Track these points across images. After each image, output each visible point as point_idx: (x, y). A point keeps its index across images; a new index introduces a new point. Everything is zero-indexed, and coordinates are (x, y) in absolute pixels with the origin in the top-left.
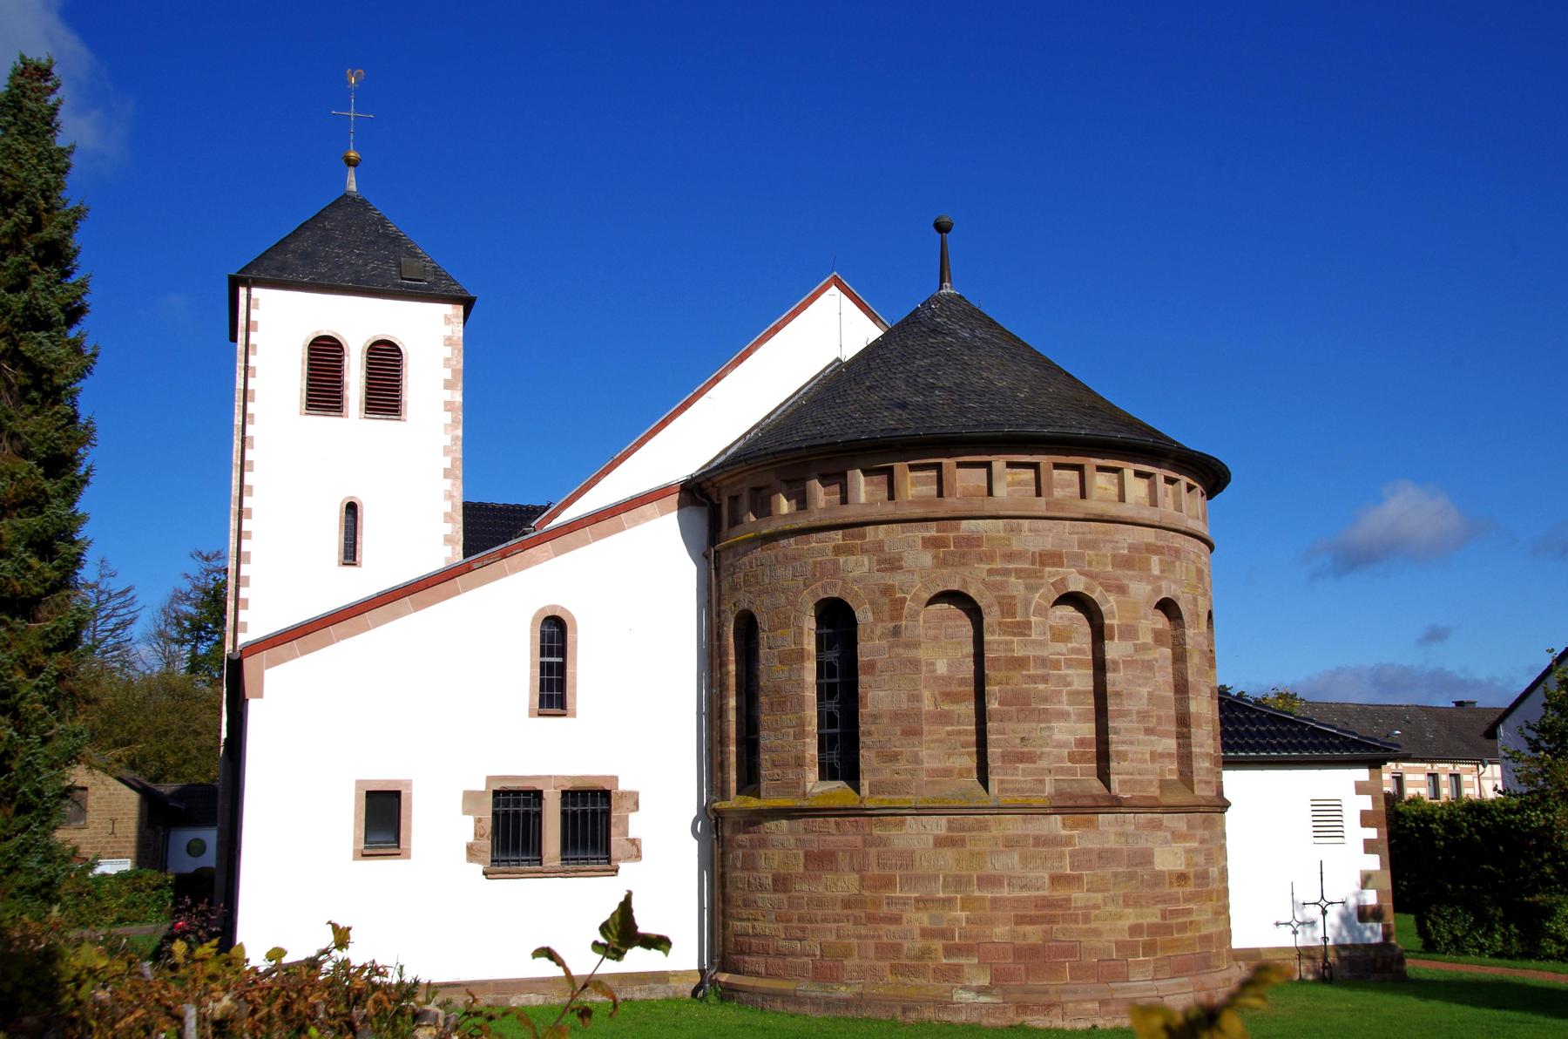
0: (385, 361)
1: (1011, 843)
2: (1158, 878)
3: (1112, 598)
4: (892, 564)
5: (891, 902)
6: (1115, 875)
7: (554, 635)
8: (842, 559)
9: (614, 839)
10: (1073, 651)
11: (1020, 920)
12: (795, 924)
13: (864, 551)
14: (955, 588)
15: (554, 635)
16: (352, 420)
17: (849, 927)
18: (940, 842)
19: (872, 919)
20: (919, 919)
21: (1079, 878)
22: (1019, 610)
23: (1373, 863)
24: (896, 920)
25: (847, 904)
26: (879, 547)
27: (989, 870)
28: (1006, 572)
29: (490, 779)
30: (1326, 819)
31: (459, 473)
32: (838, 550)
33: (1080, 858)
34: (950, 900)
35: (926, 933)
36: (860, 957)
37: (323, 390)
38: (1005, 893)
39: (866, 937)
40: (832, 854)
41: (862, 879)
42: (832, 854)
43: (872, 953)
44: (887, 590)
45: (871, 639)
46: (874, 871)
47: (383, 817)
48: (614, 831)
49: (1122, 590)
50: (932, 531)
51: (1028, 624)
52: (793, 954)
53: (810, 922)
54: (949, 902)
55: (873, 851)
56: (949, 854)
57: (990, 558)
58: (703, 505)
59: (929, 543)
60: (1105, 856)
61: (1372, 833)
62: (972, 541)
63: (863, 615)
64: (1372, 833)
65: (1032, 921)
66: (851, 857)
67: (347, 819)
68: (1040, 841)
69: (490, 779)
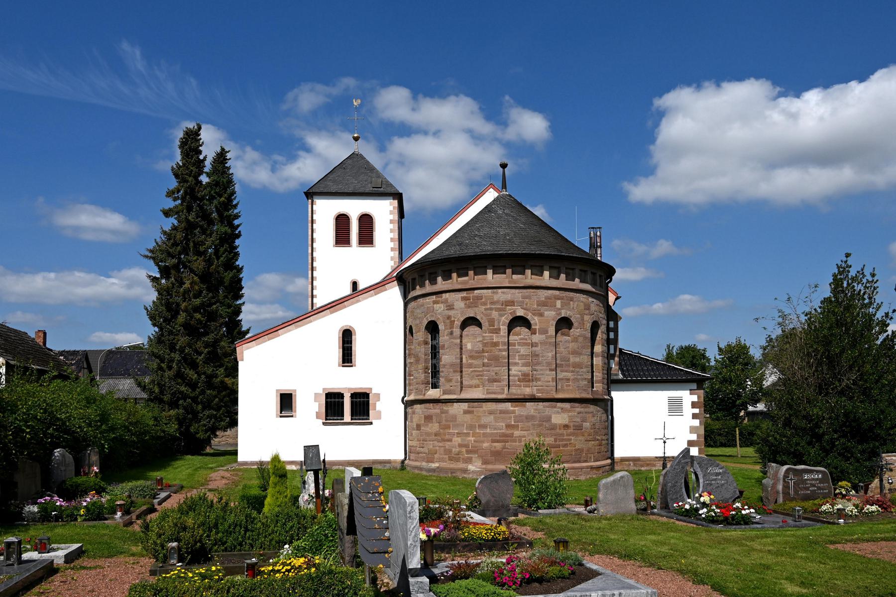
0: (366, 221)
1: (491, 413)
2: (553, 427)
3: (536, 318)
4: (450, 307)
5: (449, 434)
6: (533, 425)
7: (347, 336)
9: (371, 412)
10: (521, 339)
11: (493, 441)
14: (472, 315)
15: (347, 336)
16: (355, 250)
18: (466, 412)
19: (444, 440)
20: (457, 440)
21: (518, 426)
22: (496, 323)
23: (697, 423)
24: (450, 440)
26: (446, 301)
27: (482, 422)
28: (491, 309)
29: (324, 389)
30: (675, 407)
33: (519, 419)
34: (469, 434)
35: (460, 446)
37: (342, 238)
38: (488, 431)
44: (449, 317)
46: (444, 423)
47: (286, 402)
48: (371, 408)
49: (541, 315)
50: (464, 294)
51: (500, 329)
54: (467, 434)
55: (443, 415)
56: (468, 416)
57: (485, 304)
59: (464, 299)
60: (529, 418)
61: (697, 411)
62: (479, 298)
63: (441, 327)
64: (697, 411)
65: (498, 441)
67: (274, 403)
68: (502, 412)
69: (324, 389)
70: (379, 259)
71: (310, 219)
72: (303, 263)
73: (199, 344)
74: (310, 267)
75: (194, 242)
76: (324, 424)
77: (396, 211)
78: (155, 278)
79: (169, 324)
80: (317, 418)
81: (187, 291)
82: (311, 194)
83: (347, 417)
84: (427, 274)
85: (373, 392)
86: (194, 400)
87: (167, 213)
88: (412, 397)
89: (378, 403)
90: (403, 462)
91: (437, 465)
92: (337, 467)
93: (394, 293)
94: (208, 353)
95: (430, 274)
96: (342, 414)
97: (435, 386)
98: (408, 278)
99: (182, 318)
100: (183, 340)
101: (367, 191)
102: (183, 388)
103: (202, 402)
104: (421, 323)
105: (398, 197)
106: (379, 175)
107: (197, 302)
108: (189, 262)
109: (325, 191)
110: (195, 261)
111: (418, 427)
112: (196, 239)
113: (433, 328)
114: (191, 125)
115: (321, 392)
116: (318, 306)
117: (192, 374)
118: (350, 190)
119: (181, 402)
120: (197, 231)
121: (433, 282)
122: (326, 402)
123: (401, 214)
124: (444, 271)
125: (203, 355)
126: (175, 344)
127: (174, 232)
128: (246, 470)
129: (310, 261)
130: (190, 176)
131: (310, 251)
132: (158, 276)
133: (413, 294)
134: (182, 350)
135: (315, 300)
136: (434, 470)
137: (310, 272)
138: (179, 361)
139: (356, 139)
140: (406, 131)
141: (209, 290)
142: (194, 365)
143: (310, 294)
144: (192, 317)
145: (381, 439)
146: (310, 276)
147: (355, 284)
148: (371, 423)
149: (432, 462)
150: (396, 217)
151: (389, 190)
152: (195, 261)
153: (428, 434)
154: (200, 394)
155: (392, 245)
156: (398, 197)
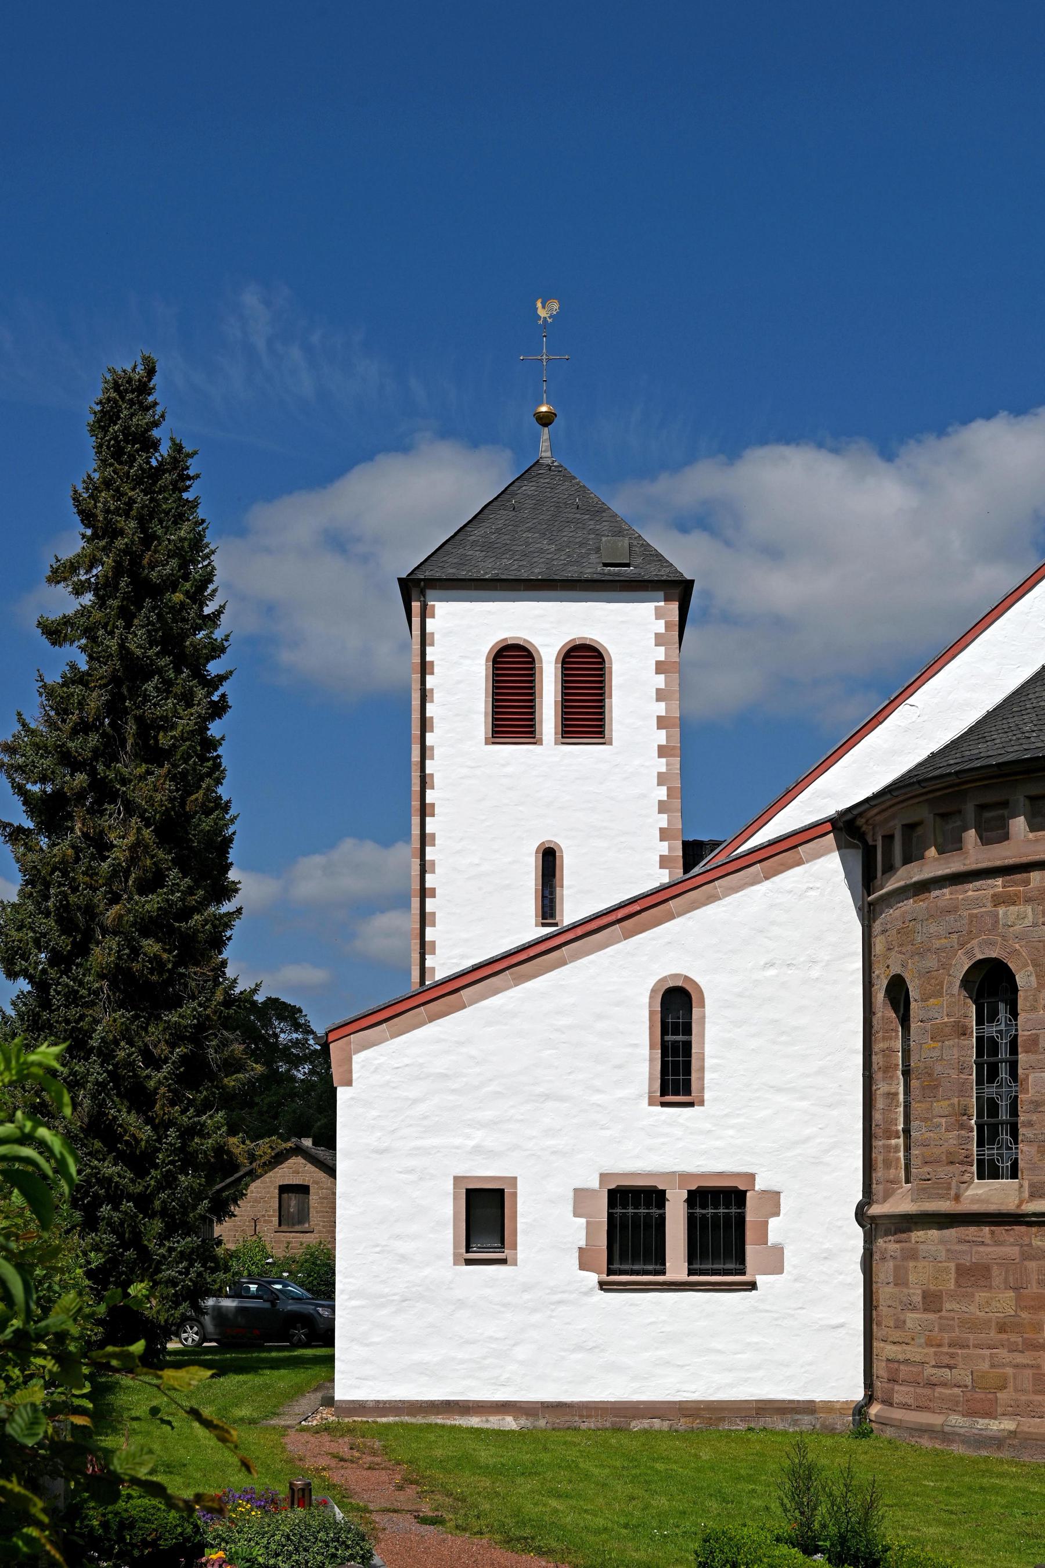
0: (585, 666)
8: (1001, 910)
9: (749, 1249)
12: (945, 1349)
13: (1028, 900)
16: (549, 755)
17: (1003, 1353)
25: (1002, 1329)
31: (677, 803)
32: (999, 900)
36: (1016, 1390)
37: (511, 715)
39: (1025, 1366)
40: (987, 1268)
41: (1018, 1298)
42: (987, 1268)
43: (1028, 1385)
45: (1034, 1009)
47: (486, 1217)
52: (944, 1385)
53: (962, 1347)
58: (855, 846)
66: (1007, 1272)
72: (396, 798)
73: (154, 1036)
74: (416, 804)
75: (140, 720)
76: (603, 1286)
78: (20, 829)
79: (66, 972)
80: (583, 1266)
81: (118, 873)
82: (416, 589)
83: (676, 1266)
84: (970, 809)
85: (759, 1186)
86: (143, 1202)
87: (55, 632)
88: (900, 1203)
89: (773, 1223)
90: (860, 1410)
91: (1008, 1425)
92: (645, 1424)
94: (184, 1059)
95: (982, 808)
96: (657, 1257)
97: (988, 1170)
99: (103, 953)
100: (107, 1022)
101: (588, 573)
102: (110, 1169)
103: (164, 1213)
104: (945, 966)
107: (152, 903)
108: (124, 782)
109: (463, 574)
110: (142, 778)
111: (931, 1301)
112: (149, 711)
113: (992, 985)
114: (127, 363)
115: (594, 1183)
117: (131, 1121)
118: (537, 572)
119: (105, 1210)
120: (149, 686)
121: (994, 831)
122: (610, 1216)
124: (1032, 799)
125: (166, 1069)
126: (89, 1034)
127: (78, 689)
128: (365, 1430)
129: (416, 787)
130: (127, 514)
131: (416, 757)
132: (29, 824)
134: (106, 1054)
136: (998, 1442)
137: (416, 820)
138: (101, 1085)
141: (182, 864)
142: (140, 1099)
143: (416, 886)
144: (135, 951)
145: (790, 1336)
146: (416, 831)
148: (752, 1286)
149: (990, 1415)
151: (652, 572)
152: (142, 778)
153: (972, 1325)
154: (160, 1188)
156: (679, 590)
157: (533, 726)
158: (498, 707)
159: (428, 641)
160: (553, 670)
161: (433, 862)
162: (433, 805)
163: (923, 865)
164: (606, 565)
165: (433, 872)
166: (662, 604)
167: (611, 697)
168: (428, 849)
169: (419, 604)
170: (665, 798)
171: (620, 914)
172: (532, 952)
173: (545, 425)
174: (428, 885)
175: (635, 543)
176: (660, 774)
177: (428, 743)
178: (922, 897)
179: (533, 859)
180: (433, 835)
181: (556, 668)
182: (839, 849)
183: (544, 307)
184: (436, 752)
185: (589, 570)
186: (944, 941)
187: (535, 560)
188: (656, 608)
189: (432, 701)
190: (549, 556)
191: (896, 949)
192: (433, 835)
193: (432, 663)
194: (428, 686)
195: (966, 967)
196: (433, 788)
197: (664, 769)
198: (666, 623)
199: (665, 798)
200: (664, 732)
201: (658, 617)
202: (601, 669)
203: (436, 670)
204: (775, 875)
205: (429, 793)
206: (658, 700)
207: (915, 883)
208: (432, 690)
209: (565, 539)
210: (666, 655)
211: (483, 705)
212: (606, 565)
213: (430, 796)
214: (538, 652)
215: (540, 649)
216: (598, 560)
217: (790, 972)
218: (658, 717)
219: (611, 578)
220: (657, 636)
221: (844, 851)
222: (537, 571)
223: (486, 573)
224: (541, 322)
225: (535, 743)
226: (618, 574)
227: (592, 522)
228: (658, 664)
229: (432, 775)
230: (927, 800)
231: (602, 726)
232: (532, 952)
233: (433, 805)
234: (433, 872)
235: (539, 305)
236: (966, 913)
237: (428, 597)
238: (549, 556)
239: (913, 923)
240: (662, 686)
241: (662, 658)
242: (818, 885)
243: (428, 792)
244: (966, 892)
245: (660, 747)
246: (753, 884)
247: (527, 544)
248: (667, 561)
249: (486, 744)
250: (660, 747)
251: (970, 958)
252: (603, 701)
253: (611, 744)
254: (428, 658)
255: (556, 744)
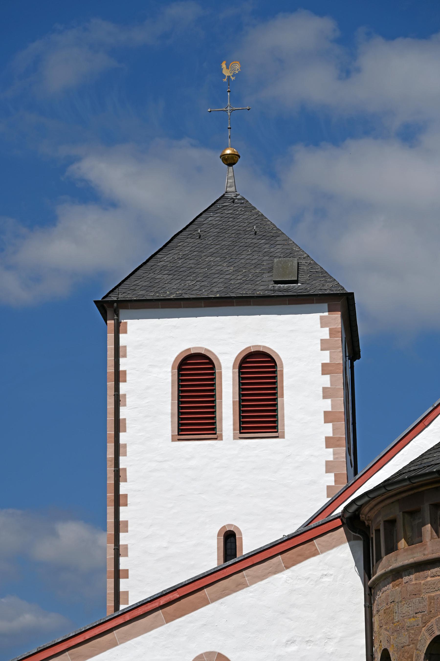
16: (229, 450)
37: (194, 414)
58: (356, 538)
70: (293, 471)
71: (111, 370)
74: (111, 495)
77: (338, 341)
82: (113, 307)
93: (339, 560)
98: (376, 520)
104: (413, 641)
105: (344, 303)
106: (291, 250)
109: (151, 295)
116: (133, 600)
118: (216, 291)
123: (352, 348)
129: (111, 481)
131: (110, 454)
133: (387, 563)
135: (124, 584)
137: (111, 510)
139: (230, 161)
140: (326, 129)
143: (111, 568)
146: (111, 519)
147: (230, 539)
150: (339, 358)
151: (317, 287)
155: (328, 430)
156: (344, 303)
157: (214, 424)
158: (244, 395)
159: (121, 354)
160: (231, 374)
161: (126, 547)
162: (126, 496)
163: (397, 555)
164: (276, 282)
165: (126, 555)
166: (326, 314)
167: (282, 396)
168: (122, 535)
169: (113, 322)
170: (333, 484)
171: (162, 601)
172: (87, 636)
173: (230, 165)
174: (122, 567)
175: (303, 262)
176: (327, 463)
177: (122, 441)
178: (397, 582)
179: (216, 541)
180: (126, 523)
181: (233, 373)
182: (349, 540)
183: (228, 68)
184: (128, 449)
185: (262, 288)
186: (412, 620)
187: (215, 280)
188: (321, 317)
189: (125, 405)
190: (228, 277)
191: (384, 627)
192: (126, 523)
193: (125, 372)
194: (121, 392)
195: (428, 642)
196: (126, 481)
197: (331, 458)
198: (330, 330)
199: (333, 484)
200: (330, 425)
201: (323, 325)
202: (275, 372)
203: (128, 378)
204: (294, 565)
205: (122, 485)
206: (324, 397)
207: (392, 571)
208: (125, 395)
209: (243, 261)
210: (331, 357)
211: (170, 407)
212: (276, 282)
213: (123, 488)
214: (217, 359)
215: (219, 356)
216: (270, 279)
217: (308, 648)
218: (325, 412)
219: (280, 294)
220: (323, 341)
221: (353, 542)
222: (215, 290)
223: (171, 293)
224: (225, 80)
225: (216, 439)
226: (287, 290)
227: (267, 246)
228: (324, 365)
229: (125, 470)
230: (398, 500)
231: (276, 422)
232: (87, 636)
233: (126, 496)
234: (126, 555)
235: (224, 65)
236: (426, 596)
237: (121, 316)
238: (228, 277)
239: (393, 604)
240: (328, 385)
241: (327, 361)
242: (331, 572)
243: (122, 485)
244: (426, 577)
245: (327, 439)
246: (275, 573)
247: (209, 267)
248: (331, 277)
249: (173, 440)
250: (327, 439)
251: (430, 635)
252: (275, 400)
253: (283, 437)
254: (121, 368)
255: (234, 439)
